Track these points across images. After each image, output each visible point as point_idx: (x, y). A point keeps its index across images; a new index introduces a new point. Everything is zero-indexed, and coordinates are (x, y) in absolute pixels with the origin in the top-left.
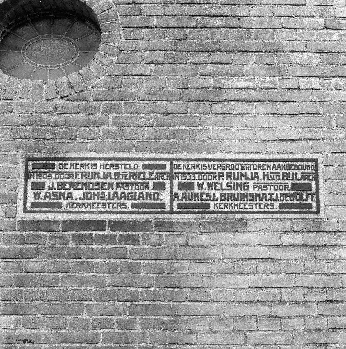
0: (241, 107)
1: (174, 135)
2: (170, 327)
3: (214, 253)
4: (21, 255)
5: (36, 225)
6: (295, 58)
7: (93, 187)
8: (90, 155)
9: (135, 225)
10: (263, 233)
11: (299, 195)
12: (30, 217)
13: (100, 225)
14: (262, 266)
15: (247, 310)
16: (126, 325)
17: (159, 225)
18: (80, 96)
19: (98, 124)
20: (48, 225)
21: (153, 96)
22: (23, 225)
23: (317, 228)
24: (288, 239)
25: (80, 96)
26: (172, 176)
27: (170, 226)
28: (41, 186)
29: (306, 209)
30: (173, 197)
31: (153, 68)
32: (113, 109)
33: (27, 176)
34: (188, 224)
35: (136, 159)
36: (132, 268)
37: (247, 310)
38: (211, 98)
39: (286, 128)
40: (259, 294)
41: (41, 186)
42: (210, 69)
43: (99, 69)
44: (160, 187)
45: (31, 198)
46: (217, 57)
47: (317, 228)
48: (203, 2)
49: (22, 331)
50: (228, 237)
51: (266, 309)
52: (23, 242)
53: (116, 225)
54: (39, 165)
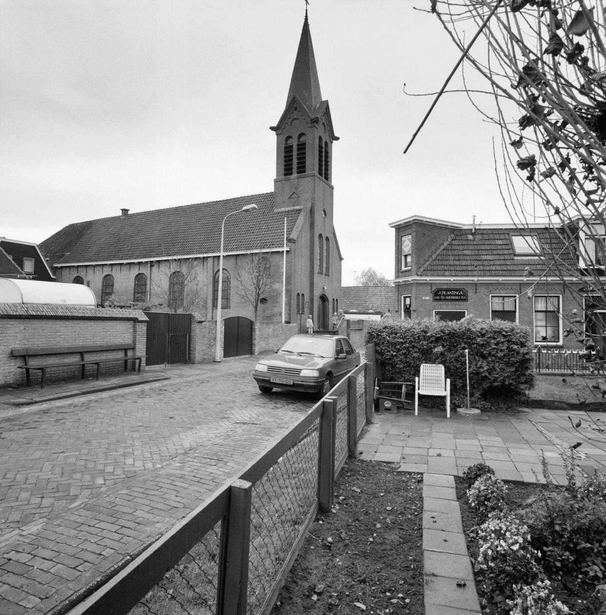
38: (275, 307)
54: (264, 312)
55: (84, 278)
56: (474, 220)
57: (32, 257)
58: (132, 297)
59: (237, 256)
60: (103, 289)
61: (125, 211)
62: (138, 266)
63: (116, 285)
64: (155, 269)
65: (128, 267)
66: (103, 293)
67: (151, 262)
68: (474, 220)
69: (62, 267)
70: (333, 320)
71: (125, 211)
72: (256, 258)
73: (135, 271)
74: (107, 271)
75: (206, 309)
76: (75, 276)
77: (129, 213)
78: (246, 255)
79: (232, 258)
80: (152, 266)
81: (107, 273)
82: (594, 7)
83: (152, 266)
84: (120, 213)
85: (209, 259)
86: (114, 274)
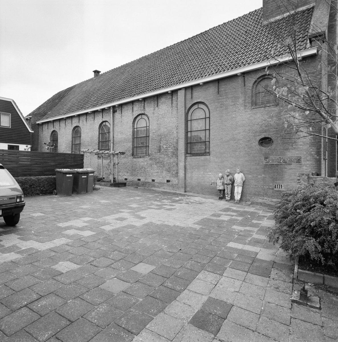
0: (291, 150)
1: (283, 154)
2: (282, 176)
3: (288, 168)
4: (264, 168)
5: (266, 165)
6: (299, 143)
7: (273, 160)
8: (272, 157)
9: (277, 165)
10: (294, 165)
11: (299, 161)
12: (265, 164)
13: (273, 165)
14: (294, 169)
15: (291, 174)
16: (277, 176)
17: (281, 165)
18: (271, 150)
19: (273, 153)
20: (267, 165)
21: (280, 149)
22: (264, 165)
23: (301, 165)
24: (297, 166)
25: (271, 150)
26: (282, 159)
27: (282, 165)
28: (266, 160)
29: (300, 162)
30: (282, 161)
31: (144, 152)
32: (275, 151)
33: (265, 159)
34: (284, 164)
35: (278, 157)
36: (277, 169)
37: (291, 174)
38: (287, 149)
39: (297, 153)
40: (293, 172)
41: (266, 160)
42: (287, 145)
43: (274, 146)
44: (281, 160)
45: (265, 162)
46: (288, 144)
47: (301, 165)
48: (58, 173)
49: (265, 176)
50: (289, 166)
51: (294, 174)
52: (265, 166)
53: (275, 165)
54: (266, 158)
55: (58, 132)
56: (205, 131)
57: (10, 112)
58: (97, 147)
59: (218, 81)
60: (72, 141)
61: (96, 72)
62: (101, 114)
63: (82, 135)
64: (118, 115)
65: (92, 116)
66: (72, 144)
67: (114, 107)
68: (205, 131)
69: (43, 123)
70: (208, 152)
71: (96, 72)
72: (251, 80)
73: (99, 119)
74: (75, 122)
75: (177, 156)
76: (52, 130)
77: (100, 73)
78: (235, 76)
79: (211, 85)
80: (114, 112)
81: (75, 125)
82: (5, 285)
83: (114, 112)
84: (92, 75)
85: (179, 92)
86: (80, 125)
